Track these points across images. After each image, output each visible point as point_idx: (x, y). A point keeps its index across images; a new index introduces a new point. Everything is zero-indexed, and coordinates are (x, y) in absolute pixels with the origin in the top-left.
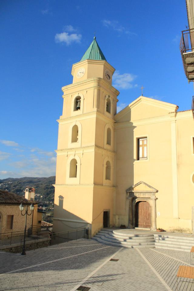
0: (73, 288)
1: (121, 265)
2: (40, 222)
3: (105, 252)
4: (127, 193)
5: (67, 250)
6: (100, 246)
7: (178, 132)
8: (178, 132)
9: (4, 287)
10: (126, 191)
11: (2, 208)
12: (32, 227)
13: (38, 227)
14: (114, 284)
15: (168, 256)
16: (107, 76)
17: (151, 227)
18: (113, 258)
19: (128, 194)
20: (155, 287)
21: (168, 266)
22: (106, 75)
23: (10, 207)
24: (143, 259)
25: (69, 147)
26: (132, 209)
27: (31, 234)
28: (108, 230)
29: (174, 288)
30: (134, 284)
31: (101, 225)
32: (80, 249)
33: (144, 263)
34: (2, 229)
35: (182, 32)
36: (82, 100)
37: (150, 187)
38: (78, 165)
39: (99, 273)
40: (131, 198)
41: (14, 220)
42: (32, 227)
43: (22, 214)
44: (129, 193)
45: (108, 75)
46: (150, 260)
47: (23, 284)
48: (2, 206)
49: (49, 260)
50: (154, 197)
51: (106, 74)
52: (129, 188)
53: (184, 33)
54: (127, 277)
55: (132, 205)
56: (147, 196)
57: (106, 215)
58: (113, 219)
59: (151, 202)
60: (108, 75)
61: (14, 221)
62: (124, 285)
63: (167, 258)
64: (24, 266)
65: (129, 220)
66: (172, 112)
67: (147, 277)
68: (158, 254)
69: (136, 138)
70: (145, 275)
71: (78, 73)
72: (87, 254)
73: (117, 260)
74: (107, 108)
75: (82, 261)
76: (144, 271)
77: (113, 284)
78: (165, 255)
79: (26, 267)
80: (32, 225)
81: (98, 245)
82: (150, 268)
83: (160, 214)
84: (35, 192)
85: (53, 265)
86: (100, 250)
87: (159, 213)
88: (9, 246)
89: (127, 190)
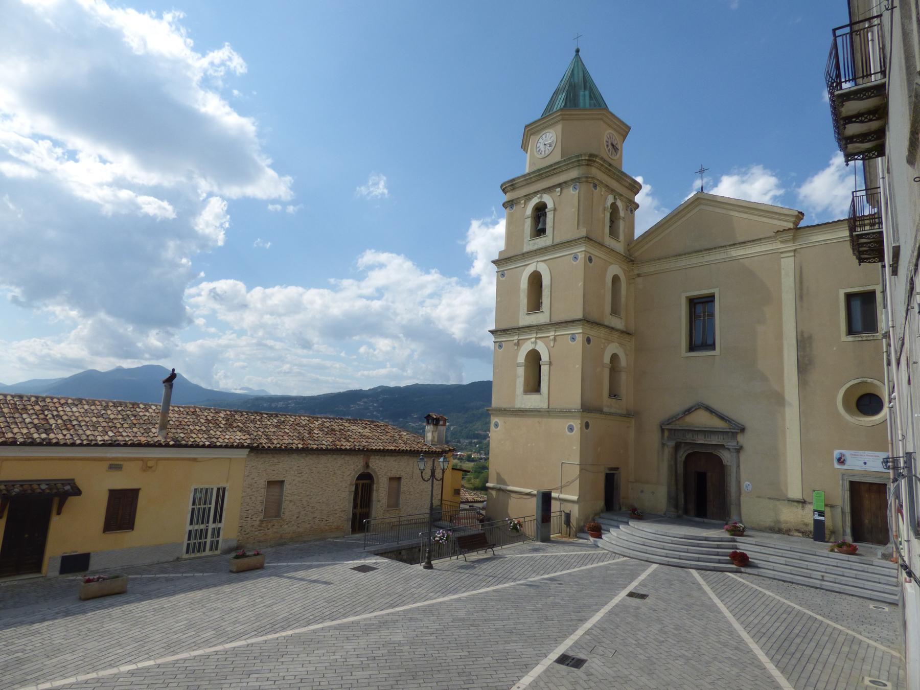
0: (546, 656)
1: (654, 611)
2: (457, 492)
3: (614, 574)
4: (663, 430)
5: (524, 561)
6: (599, 556)
7: (801, 282)
8: (801, 282)
9: (396, 639)
10: (661, 427)
11: (377, 461)
12: (441, 504)
13: (454, 504)
14: (642, 657)
15: (778, 597)
16: (610, 146)
17: (727, 518)
18: (634, 591)
19: (666, 433)
20: (748, 677)
21: (777, 624)
22: (607, 146)
23: (394, 458)
24: (710, 598)
25: (522, 323)
26: (676, 472)
27: (440, 520)
28: (615, 518)
29: (803, 681)
30: (692, 662)
31: (601, 503)
32: (554, 561)
33: (713, 608)
34: (379, 507)
35: (834, 30)
36: (550, 216)
37: (722, 417)
38: (544, 369)
39: (605, 626)
40: (672, 444)
41: (403, 488)
42: (441, 504)
43: (422, 477)
44: (670, 430)
45: (613, 145)
46: (719, 591)
47: (435, 638)
48: (377, 457)
49: (484, 584)
50: (735, 444)
51: (607, 142)
52: (669, 420)
53: (838, 33)
54: (673, 642)
55: (676, 459)
56: (714, 440)
57: (611, 481)
58: (627, 492)
59: (726, 457)
60: (613, 145)
61: (402, 490)
62: (668, 663)
63: (775, 602)
64: (431, 594)
65: (669, 498)
66: (784, 230)
67: (724, 646)
68: (746, 590)
69: (687, 297)
70: (719, 642)
71: (539, 145)
72: (570, 574)
73: (643, 596)
74: (610, 227)
75: (561, 592)
76: (716, 630)
77: (639, 656)
78: (768, 593)
79: (435, 598)
80: (442, 500)
81: (594, 554)
82: (730, 626)
83: (750, 488)
84: (342, 279)
85: (494, 596)
86: (600, 567)
87: (747, 483)
88: (394, 545)
89: (663, 424)
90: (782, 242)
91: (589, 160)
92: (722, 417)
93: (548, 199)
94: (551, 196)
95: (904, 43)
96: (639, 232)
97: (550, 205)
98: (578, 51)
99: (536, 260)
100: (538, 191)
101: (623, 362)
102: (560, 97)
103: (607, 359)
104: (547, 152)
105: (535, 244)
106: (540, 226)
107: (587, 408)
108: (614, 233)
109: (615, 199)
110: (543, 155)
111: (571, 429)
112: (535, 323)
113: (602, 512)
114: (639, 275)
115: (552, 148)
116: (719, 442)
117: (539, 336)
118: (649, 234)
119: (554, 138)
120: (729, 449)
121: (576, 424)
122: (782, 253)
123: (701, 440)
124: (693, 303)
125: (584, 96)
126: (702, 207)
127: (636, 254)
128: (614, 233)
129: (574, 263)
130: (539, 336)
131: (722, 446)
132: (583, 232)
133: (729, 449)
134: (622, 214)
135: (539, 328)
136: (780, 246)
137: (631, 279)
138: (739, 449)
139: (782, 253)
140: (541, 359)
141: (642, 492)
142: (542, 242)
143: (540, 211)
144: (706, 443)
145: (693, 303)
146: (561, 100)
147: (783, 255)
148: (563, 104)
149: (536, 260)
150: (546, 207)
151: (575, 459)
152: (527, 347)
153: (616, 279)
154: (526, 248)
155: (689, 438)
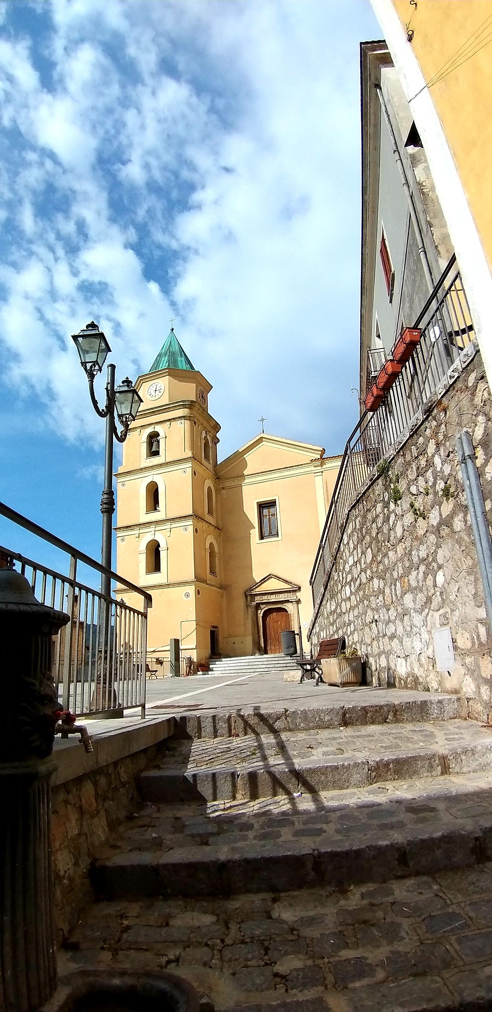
10: (245, 593)
25: (142, 521)
37: (286, 582)
38: (163, 555)
56: (282, 597)
57: (214, 635)
90: (315, 467)
91: (190, 405)
92: (286, 582)
93: (158, 429)
94: (162, 427)
95: (423, 73)
96: (220, 459)
97: (162, 434)
98: (172, 329)
99: (152, 473)
100: (152, 424)
101: (216, 550)
102: (163, 359)
103: (208, 546)
104: (157, 396)
105: (150, 462)
106: (154, 449)
107: (199, 579)
108: (207, 457)
109: (206, 434)
110: (154, 398)
111: (187, 595)
112: (153, 520)
113: (211, 658)
114: (223, 488)
115: (162, 393)
116: (284, 598)
117: (157, 529)
118: (228, 461)
119: (163, 387)
120: (292, 602)
121: (191, 589)
122: (314, 473)
123: (273, 598)
124: (262, 506)
125: (181, 361)
126: (263, 443)
127: (220, 474)
128: (207, 457)
129: (184, 475)
130: (157, 529)
131: (288, 601)
132: (190, 454)
133: (292, 602)
134: (210, 444)
135: (157, 523)
136: (313, 468)
137: (218, 491)
138: (298, 602)
139: (314, 473)
140: (160, 547)
141: (234, 643)
142: (155, 460)
143: (153, 438)
144: (277, 600)
145: (262, 506)
146: (165, 362)
147: (316, 474)
148: (167, 364)
149: (152, 473)
150: (159, 435)
151: (193, 616)
152: (147, 538)
153: (209, 489)
154: (143, 465)
155: (265, 599)
